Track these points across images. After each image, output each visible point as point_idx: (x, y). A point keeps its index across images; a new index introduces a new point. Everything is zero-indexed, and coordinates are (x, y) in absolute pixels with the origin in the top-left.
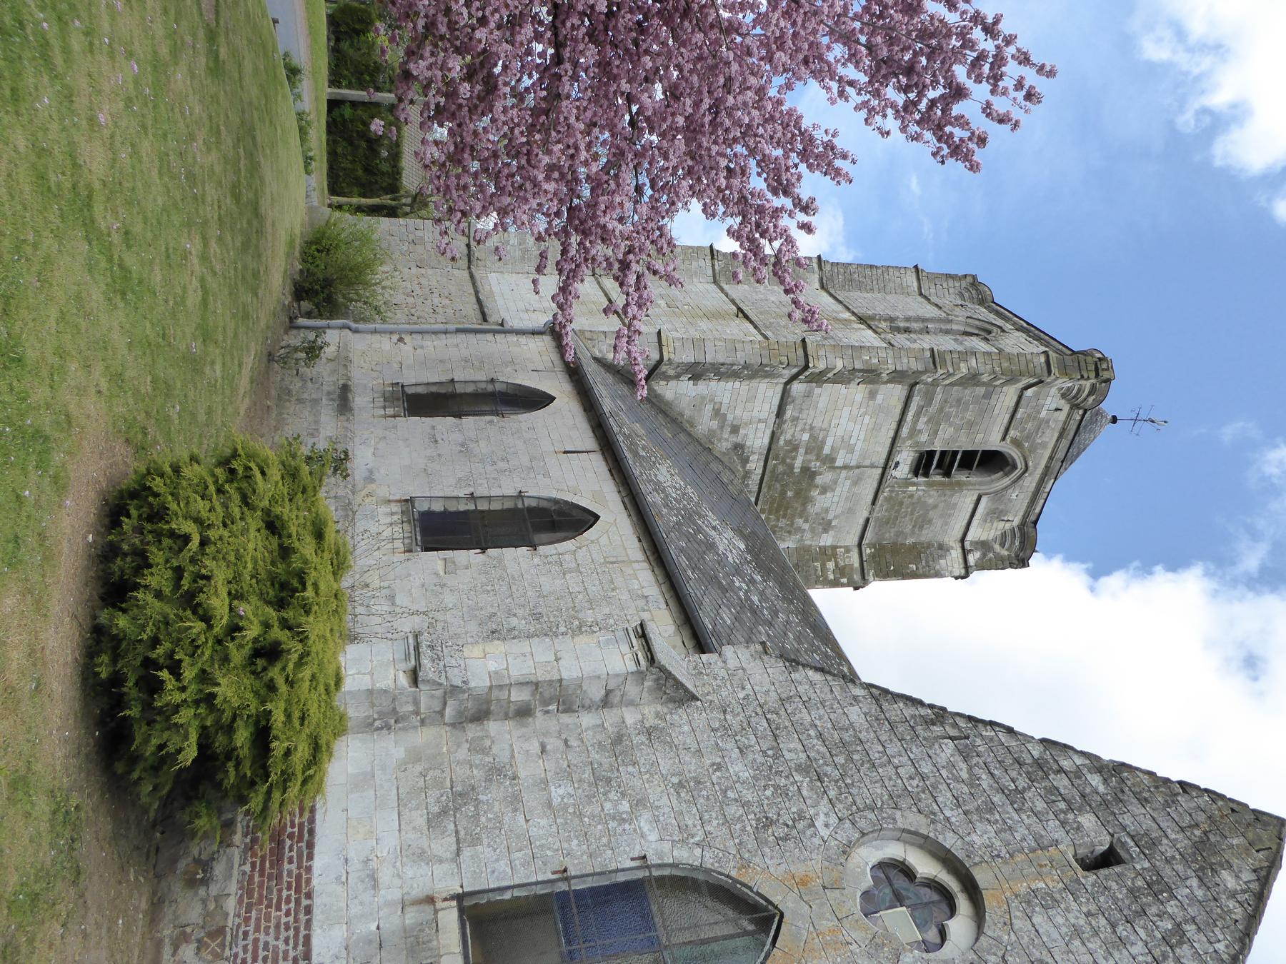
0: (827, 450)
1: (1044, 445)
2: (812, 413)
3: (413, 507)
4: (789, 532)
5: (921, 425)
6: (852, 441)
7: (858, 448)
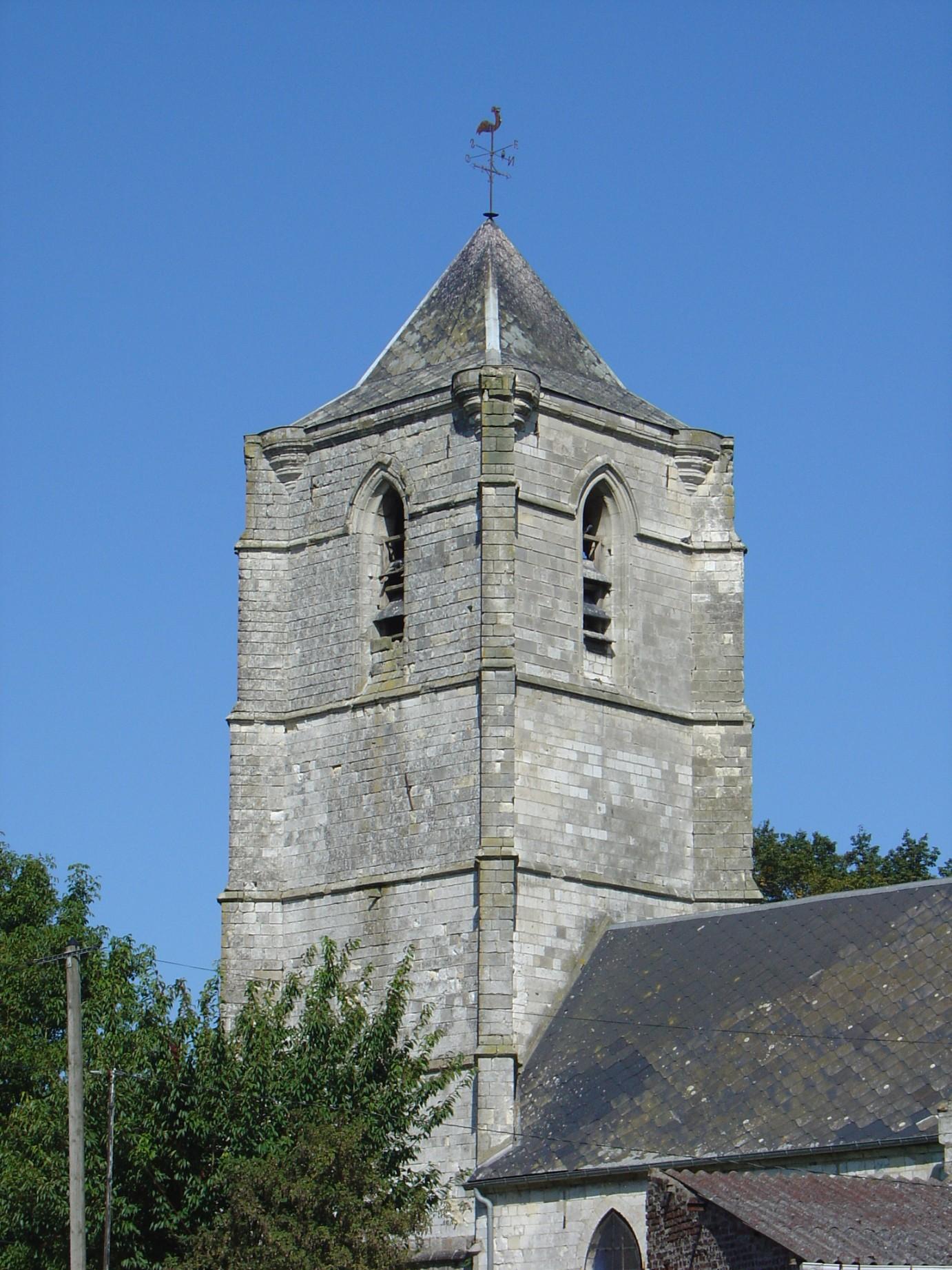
0: (583, 794)
1: (577, 441)
2: (545, 824)
3: (376, 642)
4: (675, 835)
5: (554, 654)
6: (574, 757)
7: (580, 747)
